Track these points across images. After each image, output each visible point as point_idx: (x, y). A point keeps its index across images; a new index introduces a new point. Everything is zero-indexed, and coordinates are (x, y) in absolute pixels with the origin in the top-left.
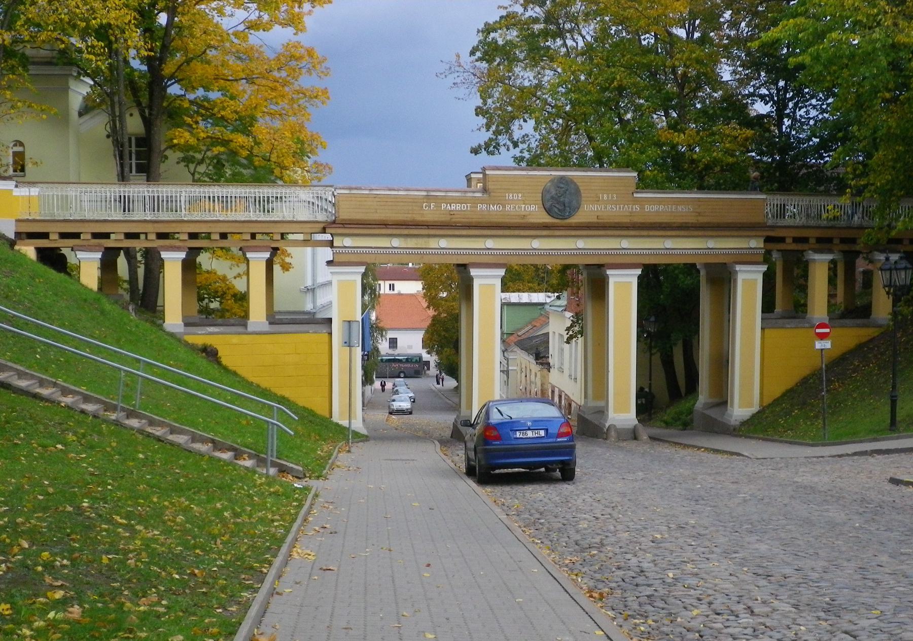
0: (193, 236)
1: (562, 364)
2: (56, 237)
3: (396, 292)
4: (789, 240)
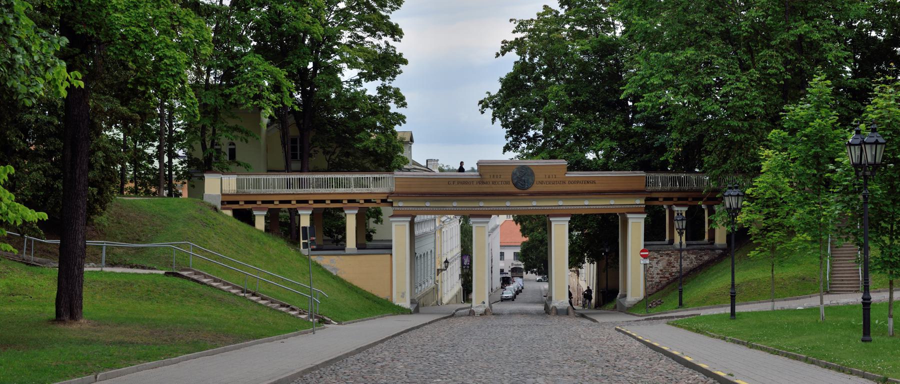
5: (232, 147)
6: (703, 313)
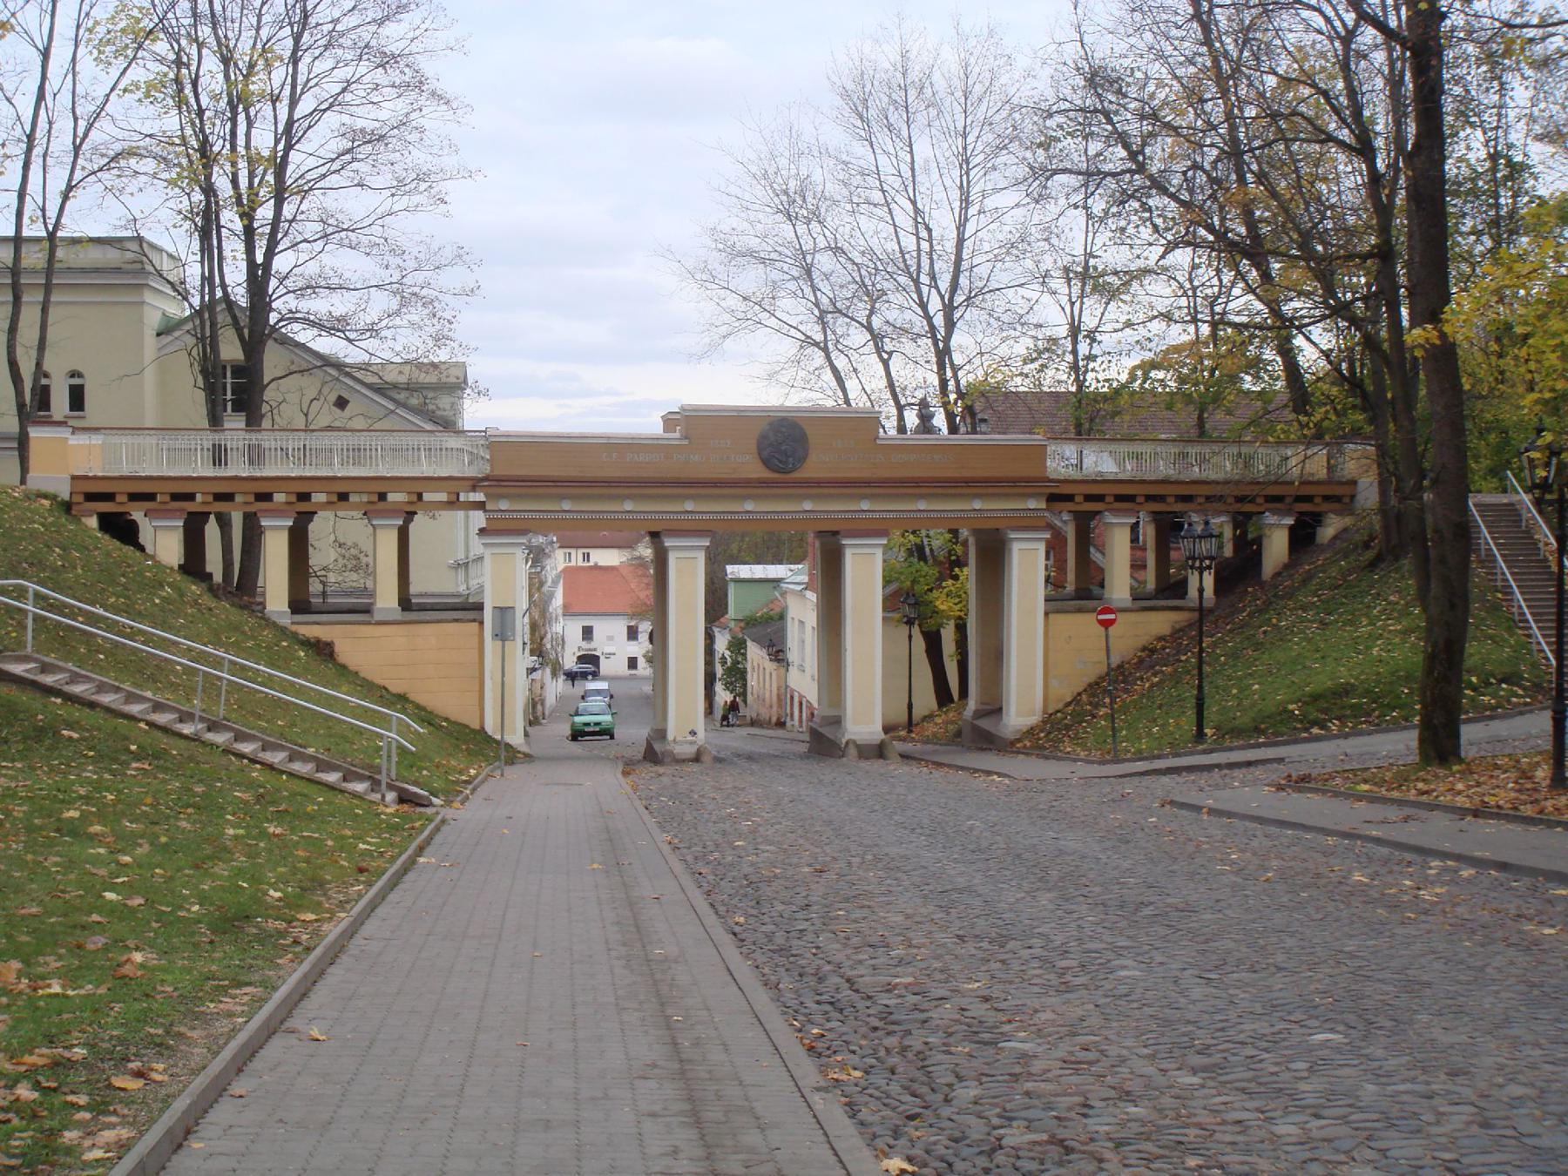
0: (1240, 499)
1: (803, 660)
2: (124, 499)
3: (591, 563)
4: (1078, 499)
5: (76, 381)
6: (101, 612)
